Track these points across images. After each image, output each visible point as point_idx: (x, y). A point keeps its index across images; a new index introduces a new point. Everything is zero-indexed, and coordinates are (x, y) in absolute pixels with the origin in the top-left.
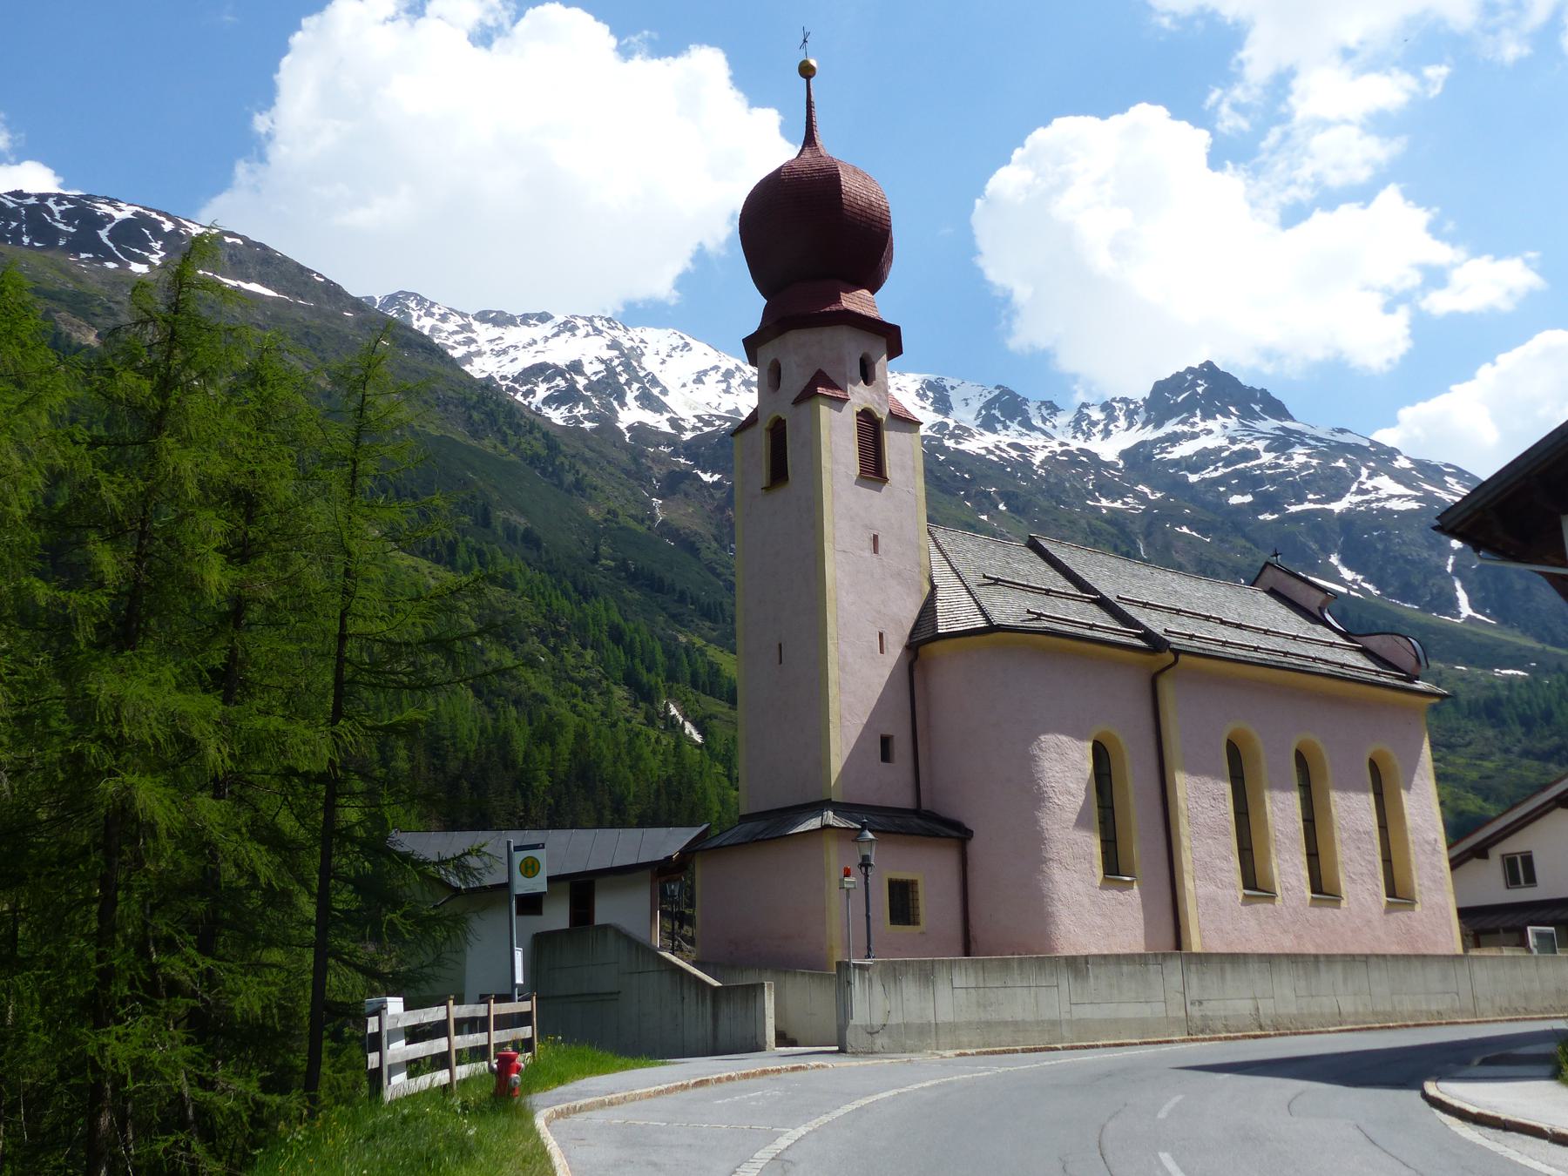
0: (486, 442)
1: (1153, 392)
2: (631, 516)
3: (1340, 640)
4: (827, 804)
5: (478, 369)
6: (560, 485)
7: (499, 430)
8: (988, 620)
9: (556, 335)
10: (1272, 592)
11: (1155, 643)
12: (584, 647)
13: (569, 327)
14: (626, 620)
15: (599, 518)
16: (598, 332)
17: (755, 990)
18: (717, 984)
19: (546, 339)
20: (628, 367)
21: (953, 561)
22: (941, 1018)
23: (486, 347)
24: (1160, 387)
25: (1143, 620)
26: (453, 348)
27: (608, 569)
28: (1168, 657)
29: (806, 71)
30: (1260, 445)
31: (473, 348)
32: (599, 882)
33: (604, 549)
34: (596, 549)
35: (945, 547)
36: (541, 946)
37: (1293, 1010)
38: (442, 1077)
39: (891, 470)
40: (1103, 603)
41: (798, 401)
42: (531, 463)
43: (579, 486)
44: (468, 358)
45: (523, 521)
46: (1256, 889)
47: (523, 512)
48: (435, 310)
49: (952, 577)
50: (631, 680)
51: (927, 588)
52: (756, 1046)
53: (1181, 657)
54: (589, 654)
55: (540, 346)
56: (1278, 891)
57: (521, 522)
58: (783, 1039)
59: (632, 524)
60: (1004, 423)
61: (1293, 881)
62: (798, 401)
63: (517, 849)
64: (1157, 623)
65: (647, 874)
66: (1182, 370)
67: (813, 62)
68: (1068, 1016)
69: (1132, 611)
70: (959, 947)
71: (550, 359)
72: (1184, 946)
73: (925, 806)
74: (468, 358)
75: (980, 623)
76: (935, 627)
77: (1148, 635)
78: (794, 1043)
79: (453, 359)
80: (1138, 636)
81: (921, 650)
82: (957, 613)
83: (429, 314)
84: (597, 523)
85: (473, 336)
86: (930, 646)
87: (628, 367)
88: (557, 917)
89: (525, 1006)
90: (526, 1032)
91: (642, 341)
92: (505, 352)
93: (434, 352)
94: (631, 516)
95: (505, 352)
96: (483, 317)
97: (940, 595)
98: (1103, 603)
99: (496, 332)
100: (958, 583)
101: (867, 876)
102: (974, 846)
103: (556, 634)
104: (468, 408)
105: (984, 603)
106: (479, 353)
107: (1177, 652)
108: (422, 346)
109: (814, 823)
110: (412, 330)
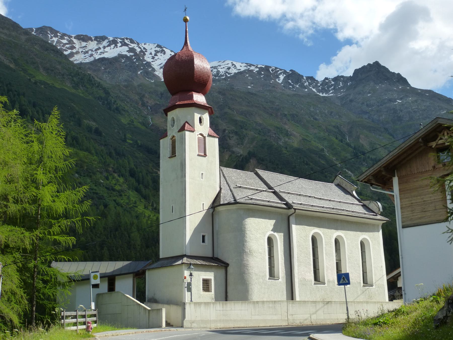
0: (79, 91)
1: (354, 74)
2: (139, 122)
3: (358, 203)
4: (185, 256)
5: (78, 59)
6: (110, 109)
7: (85, 86)
8: (235, 200)
9: (109, 46)
10: (338, 186)
11: (289, 206)
12: (119, 176)
13: (114, 42)
14: (137, 168)
15: (126, 123)
16: (126, 45)
17: (160, 310)
18: (149, 309)
19: (104, 47)
20: (138, 59)
21: (228, 180)
22: (211, 319)
23: (80, 50)
24: (357, 72)
25: (286, 199)
26: (66, 51)
27: (130, 144)
28: (292, 211)
29: (186, 20)
30: (395, 96)
31: (74, 51)
32: (117, 277)
33: (128, 136)
34: (125, 136)
35: (226, 175)
36: (98, 298)
37: (322, 318)
38: (75, 328)
39: (207, 153)
40: (275, 193)
41: (179, 131)
42: (98, 99)
43: (117, 109)
44: (72, 55)
45: (94, 124)
46: (319, 281)
47: (94, 120)
48: (58, 34)
49: (227, 186)
50: (137, 190)
51: (218, 189)
52: (160, 326)
53: (297, 211)
54: (121, 180)
55: (102, 50)
56: (326, 282)
57: (94, 125)
58: (168, 324)
59: (140, 126)
60: (292, 85)
61: (331, 279)
62: (179, 131)
63: (92, 272)
64: (290, 199)
65: (132, 275)
66: (366, 65)
67: (188, 18)
68: (251, 319)
69: (283, 195)
70: (224, 299)
71: (106, 55)
72: (294, 298)
73: (215, 256)
74: (72, 55)
75: (232, 200)
76: (220, 202)
77: (287, 204)
78: (172, 326)
79: (66, 56)
80: (284, 204)
81: (216, 208)
82: (226, 198)
83: (56, 36)
84: (125, 125)
85: (74, 45)
86: (218, 207)
87: (138, 59)
88: (104, 287)
89: (95, 313)
90: (95, 319)
91: (144, 48)
92: (87, 52)
93: (59, 53)
94: (139, 122)
95: (87, 52)
96: (79, 38)
97: (222, 192)
98: (275, 193)
99: (84, 44)
100: (228, 188)
101: (191, 279)
102: (230, 269)
103: (107, 171)
104: (72, 77)
105: (235, 195)
106: (77, 53)
107: (295, 209)
108: (53, 50)
109: (180, 262)
110: (49, 43)
